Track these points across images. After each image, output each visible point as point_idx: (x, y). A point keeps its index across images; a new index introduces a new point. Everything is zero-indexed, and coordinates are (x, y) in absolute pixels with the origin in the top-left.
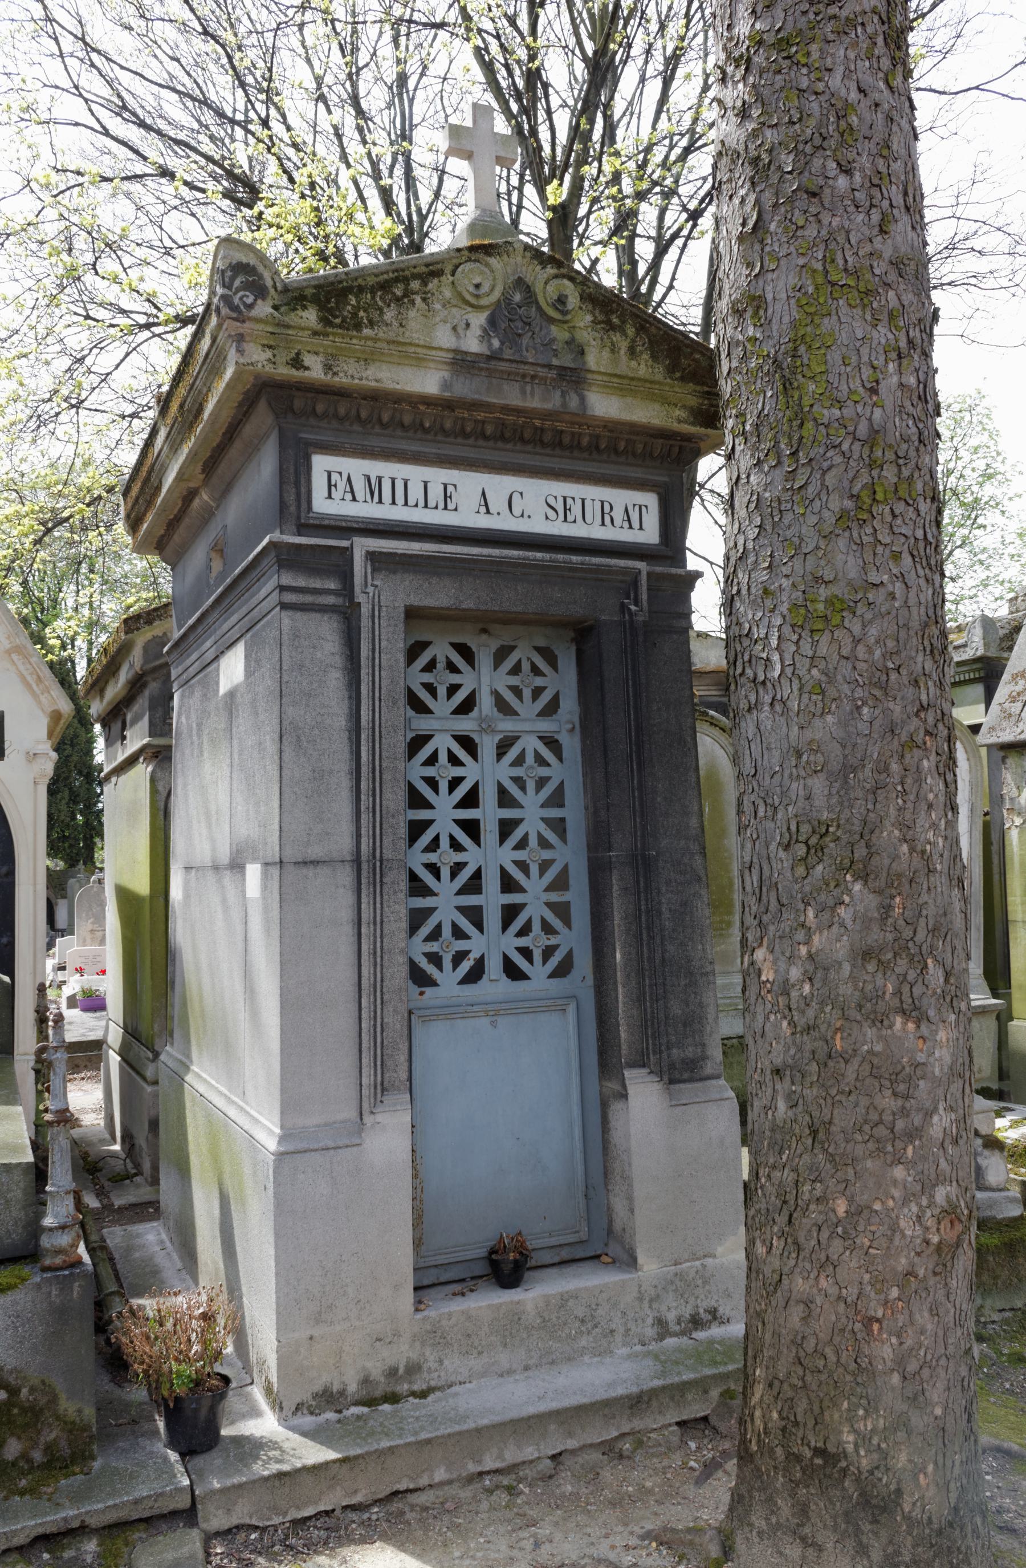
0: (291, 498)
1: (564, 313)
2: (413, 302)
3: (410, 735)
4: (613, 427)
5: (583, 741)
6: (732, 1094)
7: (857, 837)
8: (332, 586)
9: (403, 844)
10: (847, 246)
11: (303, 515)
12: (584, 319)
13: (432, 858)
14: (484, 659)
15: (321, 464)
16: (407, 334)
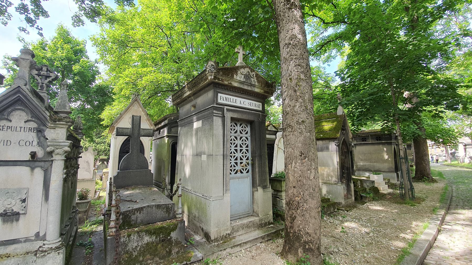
14: (239, 125)
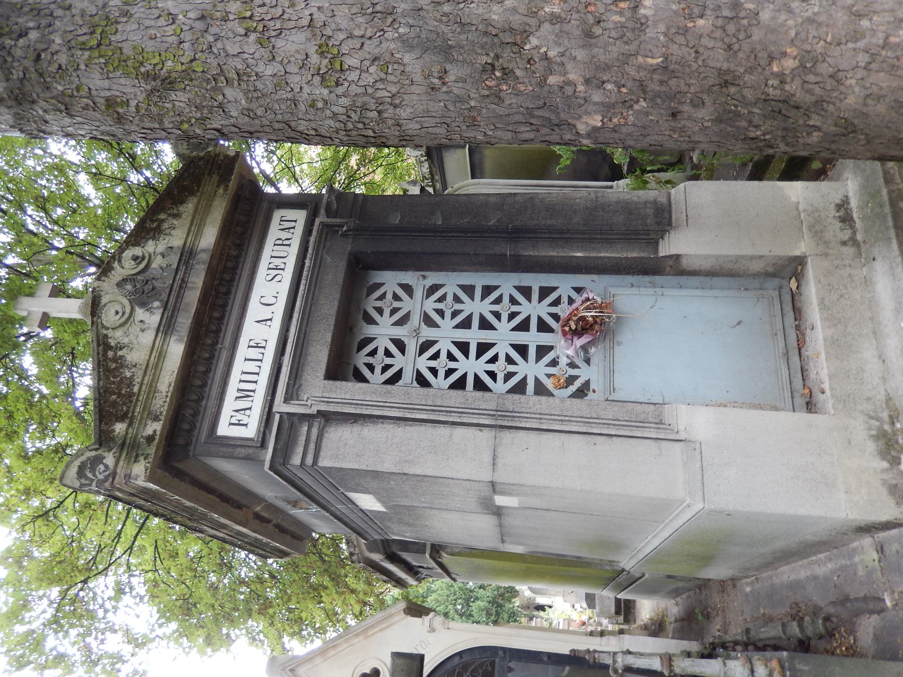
0: (243, 452)
1: (143, 258)
2: (122, 357)
3: (415, 384)
4: (225, 231)
5: (431, 270)
6: (682, 185)
7: (496, 40)
8: (306, 428)
9: (487, 395)
10: (74, 33)
11: (255, 445)
12: (150, 246)
13: (500, 377)
15: (223, 429)
16: (141, 362)
